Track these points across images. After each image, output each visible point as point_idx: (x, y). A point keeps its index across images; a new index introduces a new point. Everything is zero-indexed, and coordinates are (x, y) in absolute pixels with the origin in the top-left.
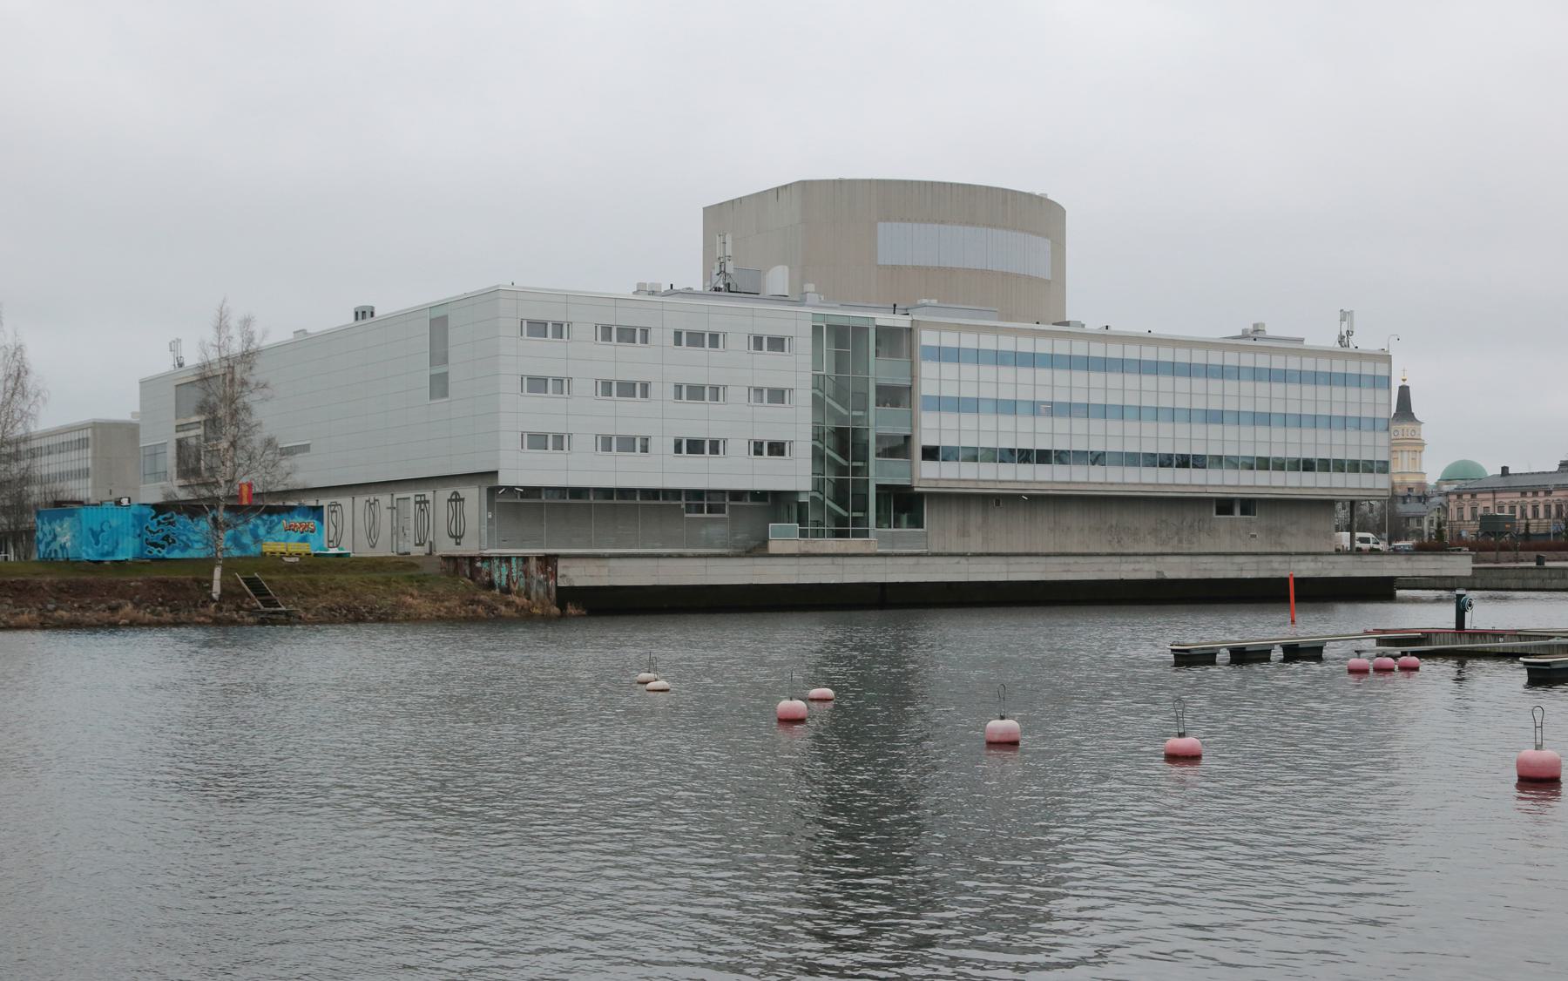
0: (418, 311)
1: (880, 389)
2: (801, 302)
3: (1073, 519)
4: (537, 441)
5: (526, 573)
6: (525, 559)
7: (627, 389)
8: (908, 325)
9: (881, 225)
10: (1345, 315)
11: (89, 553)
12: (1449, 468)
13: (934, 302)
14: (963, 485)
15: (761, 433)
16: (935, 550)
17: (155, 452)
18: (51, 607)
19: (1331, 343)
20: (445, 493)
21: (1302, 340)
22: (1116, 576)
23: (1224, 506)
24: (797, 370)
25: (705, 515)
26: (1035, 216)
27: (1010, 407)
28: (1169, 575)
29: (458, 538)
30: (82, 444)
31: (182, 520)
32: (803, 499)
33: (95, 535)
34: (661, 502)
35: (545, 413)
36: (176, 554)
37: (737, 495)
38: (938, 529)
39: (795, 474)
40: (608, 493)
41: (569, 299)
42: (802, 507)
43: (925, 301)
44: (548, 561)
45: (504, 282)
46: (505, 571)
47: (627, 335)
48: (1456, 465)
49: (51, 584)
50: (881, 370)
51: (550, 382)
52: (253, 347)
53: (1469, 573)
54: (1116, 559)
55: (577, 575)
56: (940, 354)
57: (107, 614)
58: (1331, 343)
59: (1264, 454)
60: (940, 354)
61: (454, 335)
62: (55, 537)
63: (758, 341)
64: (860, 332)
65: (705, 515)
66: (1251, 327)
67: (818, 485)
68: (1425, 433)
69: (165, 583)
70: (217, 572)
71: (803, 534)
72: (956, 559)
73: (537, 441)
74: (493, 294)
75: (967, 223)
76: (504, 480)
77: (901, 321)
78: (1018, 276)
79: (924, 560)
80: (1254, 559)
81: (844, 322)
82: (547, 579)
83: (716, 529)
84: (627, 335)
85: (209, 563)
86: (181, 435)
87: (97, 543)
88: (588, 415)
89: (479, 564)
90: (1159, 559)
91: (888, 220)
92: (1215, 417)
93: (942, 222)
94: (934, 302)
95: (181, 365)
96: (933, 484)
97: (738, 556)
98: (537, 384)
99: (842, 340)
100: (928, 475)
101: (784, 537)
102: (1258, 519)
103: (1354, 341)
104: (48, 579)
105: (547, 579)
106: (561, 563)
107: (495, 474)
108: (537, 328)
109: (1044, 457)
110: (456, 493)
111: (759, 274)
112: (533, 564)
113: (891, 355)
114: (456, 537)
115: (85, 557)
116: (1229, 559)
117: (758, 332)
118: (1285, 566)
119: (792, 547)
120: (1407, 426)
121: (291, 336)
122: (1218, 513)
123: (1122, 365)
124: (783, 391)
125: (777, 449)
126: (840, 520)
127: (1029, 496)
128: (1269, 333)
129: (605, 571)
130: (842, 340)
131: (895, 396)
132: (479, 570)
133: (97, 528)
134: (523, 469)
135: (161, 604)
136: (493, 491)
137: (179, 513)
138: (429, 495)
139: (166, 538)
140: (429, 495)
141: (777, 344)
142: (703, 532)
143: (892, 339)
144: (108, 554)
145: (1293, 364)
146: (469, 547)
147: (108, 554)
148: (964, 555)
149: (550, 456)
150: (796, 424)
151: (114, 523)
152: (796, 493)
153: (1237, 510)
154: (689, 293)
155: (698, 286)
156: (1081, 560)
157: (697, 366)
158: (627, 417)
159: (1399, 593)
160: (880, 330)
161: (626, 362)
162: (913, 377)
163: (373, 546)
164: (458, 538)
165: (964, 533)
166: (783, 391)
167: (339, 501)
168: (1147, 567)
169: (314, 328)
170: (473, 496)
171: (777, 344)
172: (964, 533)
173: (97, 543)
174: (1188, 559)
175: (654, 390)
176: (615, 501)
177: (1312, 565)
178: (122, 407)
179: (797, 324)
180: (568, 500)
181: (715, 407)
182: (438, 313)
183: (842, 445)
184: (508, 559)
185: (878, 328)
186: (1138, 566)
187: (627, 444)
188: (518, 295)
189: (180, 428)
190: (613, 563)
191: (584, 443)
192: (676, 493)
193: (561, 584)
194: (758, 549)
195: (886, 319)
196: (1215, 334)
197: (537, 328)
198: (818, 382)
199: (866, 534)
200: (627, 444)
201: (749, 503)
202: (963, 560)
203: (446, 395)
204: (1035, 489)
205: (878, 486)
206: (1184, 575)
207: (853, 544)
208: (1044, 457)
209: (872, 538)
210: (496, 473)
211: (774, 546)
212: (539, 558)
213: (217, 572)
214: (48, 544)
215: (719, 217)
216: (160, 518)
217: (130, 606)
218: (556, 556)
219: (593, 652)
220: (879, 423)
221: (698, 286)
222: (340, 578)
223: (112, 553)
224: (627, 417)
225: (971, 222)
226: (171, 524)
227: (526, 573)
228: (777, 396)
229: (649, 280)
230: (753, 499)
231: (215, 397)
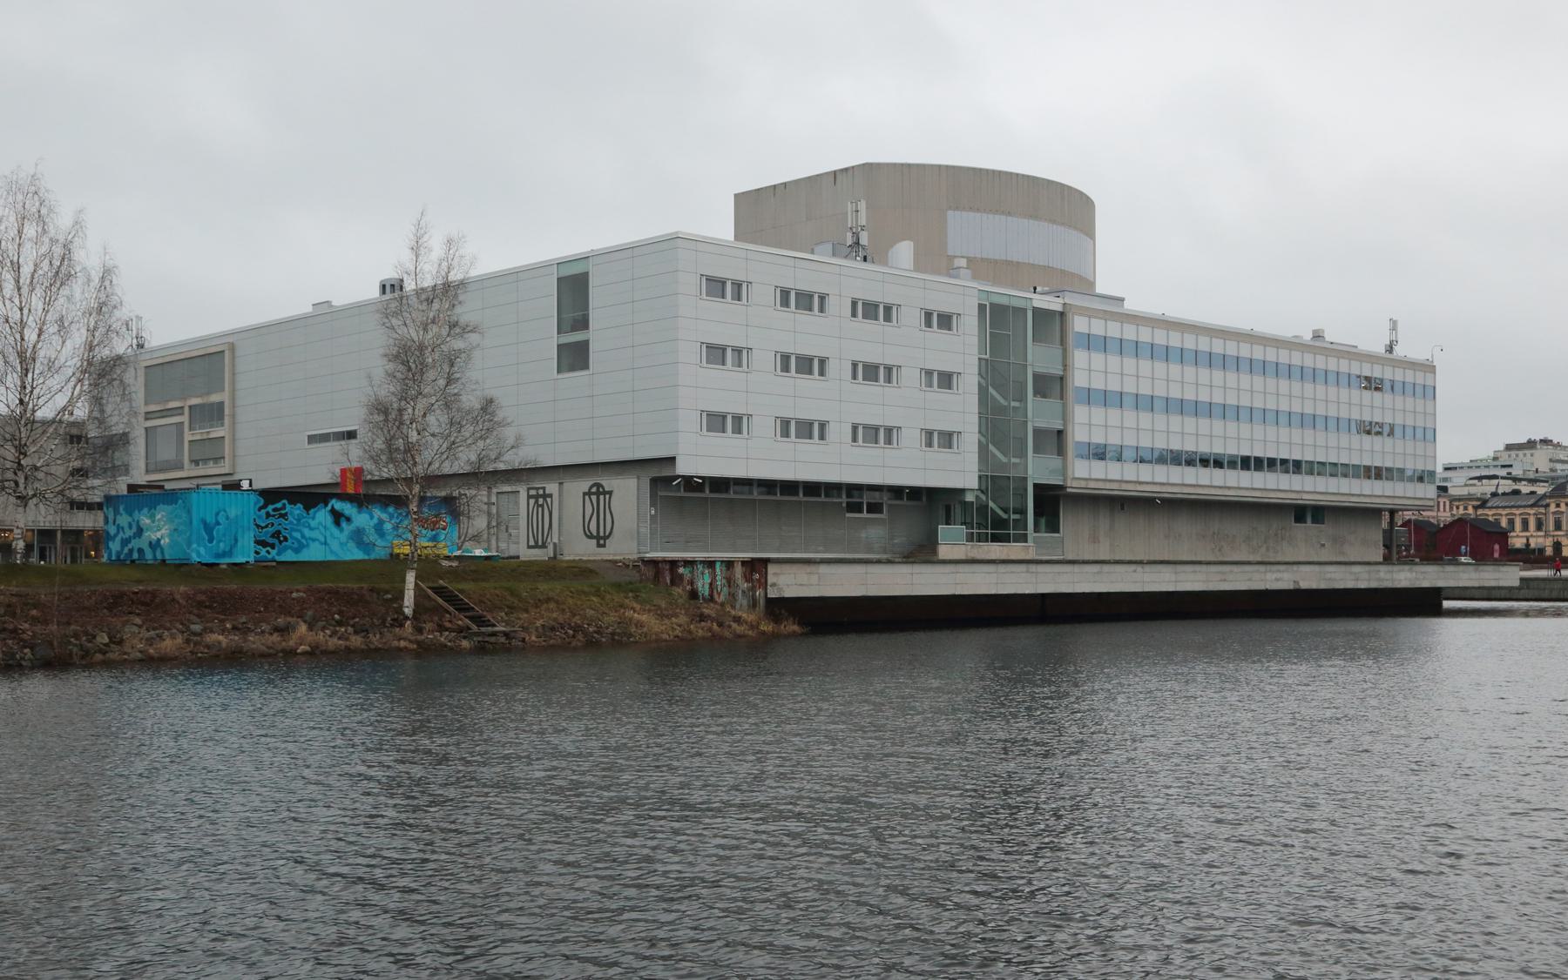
0: (546, 266)
1: (1038, 378)
3: (1185, 526)
6: (729, 564)
8: (1059, 308)
9: (950, 213)
10: (1394, 325)
11: (200, 553)
14: (1108, 486)
16: (1070, 557)
18: (197, 628)
19: (1380, 349)
20: (577, 487)
23: (1302, 513)
24: (962, 351)
28: (1304, 585)
29: (601, 540)
31: (296, 510)
32: (970, 498)
33: (209, 529)
34: (823, 499)
35: (721, 389)
36: (289, 556)
37: (897, 491)
38: (1075, 533)
39: (959, 471)
40: (768, 485)
42: (966, 506)
44: (756, 567)
46: (707, 580)
49: (187, 597)
50: (1040, 358)
51: (729, 351)
52: (455, 276)
53: (1517, 583)
54: (1262, 568)
55: (789, 583)
56: (1089, 342)
57: (276, 637)
58: (1380, 349)
59: (1367, 462)
60: (1089, 342)
62: (140, 532)
65: (865, 515)
69: (335, 593)
70: (411, 577)
71: (970, 538)
72: (1133, 567)
74: (673, 240)
75: (1031, 217)
76: (683, 468)
77: (1054, 304)
78: (1073, 275)
79: (1106, 568)
80: (1367, 568)
82: (753, 589)
83: (875, 532)
85: (396, 564)
87: (211, 541)
88: (765, 394)
89: (681, 570)
90: (1295, 568)
91: (957, 208)
92: (1308, 421)
93: (1009, 214)
95: (141, 346)
96: (1083, 484)
97: (889, 562)
98: (716, 353)
100: (1083, 473)
101: (952, 541)
102: (1327, 529)
103: (1399, 351)
104: (182, 588)
105: (753, 589)
107: (671, 460)
108: (716, 286)
110: (598, 485)
113: (1429, 393)
114: (598, 538)
115: (195, 558)
116: (1348, 568)
117: (930, 307)
118: (1388, 576)
119: (959, 552)
121: (309, 309)
127: (1164, 500)
133: (210, 519)
134: (703, 457)
135: (340, 623)
136: (656, 482)
137: (292, 502)
138: (552, 488)
139: (277, 534)
140: (552, 488)
142: (863, 535)
144: (224, 555)
147: (224, 555)
148: (1140, 562)
150: (961, 411)
151: (233, 513)
152: (962, 491)
156: (1235, 568)
159: (1447, 604)
162: (1065, 366)
164: (601, 540)
165: (1095, 540)
168: (1286, 576)
169: (338, 301)
170: (627, 493)
171: (946, 321)
172: (1095, 540)
173: (211, 541)
174: (1317, 568)
176: (732, 495)
177: (1409, 575)
179: (963, 296)
180: (779, 497)
181: (889, 391)
184: (711, 564)
185: (1035, 309)
186: (1279, 575)
187: (806, 429)
190: (823, 569)
191: (763, 426)
194: (923, 552)
200: (806, 429)
202: (1139, 568)
203: (585, 366)
205: (1036, 486)
209: (1030, 543)
210: (672, 460)
211: (944, 551)
212: (744, 563)
213: (411, 577)
214: (125, 542)
216: (270, 508)
217: (303, 628)
218: (766, 561)
222: (543, 586)
223: (230, 553)
225: (1034, 216)
226: (284, 516)
227: (730, 581)
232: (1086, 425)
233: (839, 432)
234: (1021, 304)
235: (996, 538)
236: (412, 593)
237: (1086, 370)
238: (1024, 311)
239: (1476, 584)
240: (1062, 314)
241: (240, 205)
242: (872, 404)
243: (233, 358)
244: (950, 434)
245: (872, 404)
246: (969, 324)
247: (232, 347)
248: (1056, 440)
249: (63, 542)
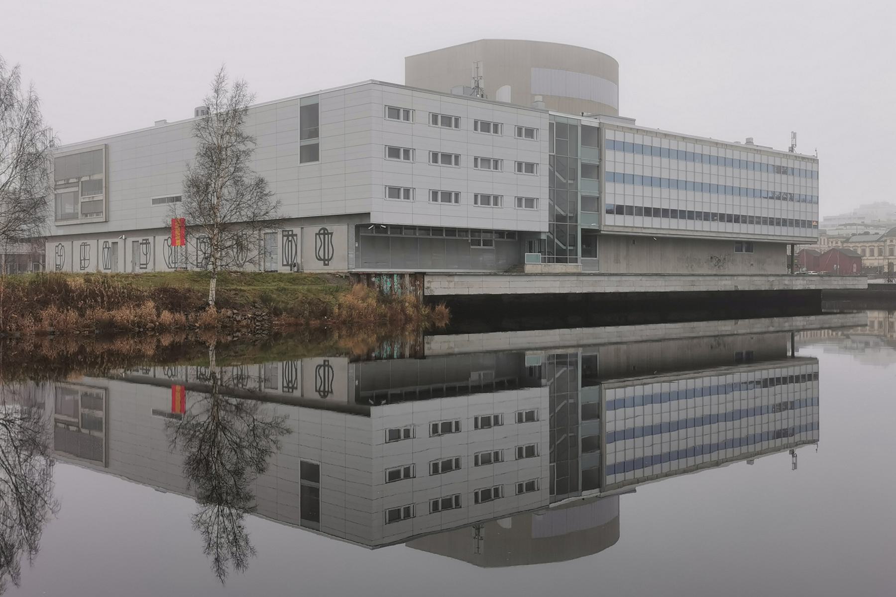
4: (394, 192)
5: (402, 286)
6: (402, 276)
14: (735, 236)
25: (482, 247)
27: (652, 182)
32: (543, 237)
35: (398, 173)
37: (501, 233)
39: (537, 221)
44: (417, 277)
54: (716, 278)
56: (614, 145)
58: (785, 149)
60: (614, 145)
63: (435, 118)
65: (482, 247)
73: (394, 192)
76: (374, 220)
77: (594, 123)
81: (564, 121)
88: (422, 176)
89: (373, 279)
94: (855, 266)
97: (495, 275)
100: (612, 223)
101: (533, 262)
106: (427, 279)
109: (737, 219)
110: (325, 229)
112: (407, 279)
113: (814, 175)
114: (324, 260)
123: (669, 153)
126: (561, 252)
129: (452, 285)
131: (593, 171)
132: (373, 283)
134: (388, 213)
140: (297, 230)
141: (530, 133)
145: (629, 138)
149: (400, 204)
150: (538, 186)
152: (540, 233)
164: (326, 261)
171: (530, 133)
172: (617, 261)
184: (391, 276)
187: (447, 197)
193: (427, 293)
194: (516, 268)
195: (586, 121)
196: (730, 139)
199: (576, 261)
200: (447, 197)
206: (557, 291)
207: (570, 267)
208: (737, 219)
211: (528, 268)
212: (411, 275)
218: (424, 274)
227: (402, 286)
235: (559, 261)
240: (598, 129)
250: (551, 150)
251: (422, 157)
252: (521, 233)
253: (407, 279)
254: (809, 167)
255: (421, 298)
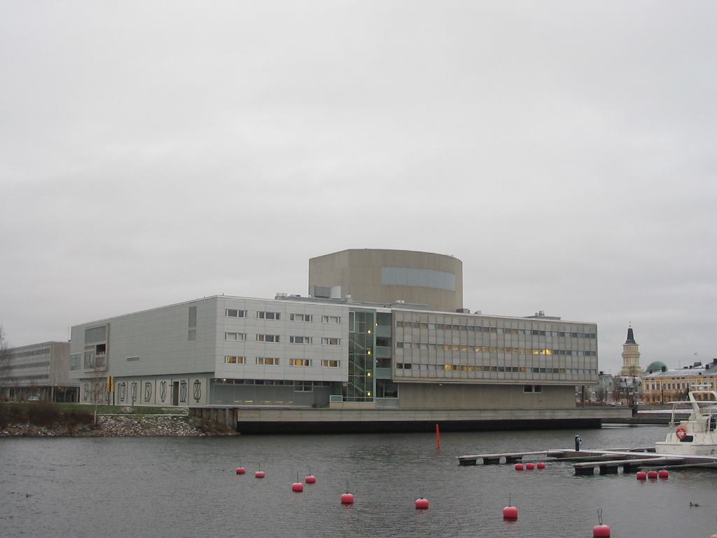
2: (344, 302)
7: (270, 338)
12: (658, 362)
13: (403, 302)
15: (327, 359)
17: (77, 357)
20: (193, 381)
21: (559, 318)
22: (479, 419)
23: (528, 388)
24: (342, 331)
26: (447, 266)
29: (198, 399)
30: (47, 351)
32: (345, 385)
37: (316, 383)
41: (245, 301)
43: (399, 301)
44: (234, 411)
45: (218, 293)
47: (270, 316)
48: (652, 365)
55: (243, 417)
60: (401, 324)
61: (199, 315)
64: (370, 315)
66: (538, 312)
67: (351, 379)
68: (640, 349)
74: (213, 300)
76: (217, 376)
77: (388, 310)
81: (363, 311)
84: (270, 316)
86: (86, 351)
94: (403, 302)
99: (362, 318)
100: (399, 375)
101: (336, 402)
106: (239, 412)
108: (232, 313)
110: (197, 381)
111: (329, 290)
112: (227, 412)
113: (594, 336)
120: (633, 347)
122: (525, 391)
124: (336, 340)
125: (334, 364)
128: (546, 315)
130: (362, 318)
134: (226, 372)
136: (212, 381)
138: (187, 381)
143: (385, 319)
146: (203, 404)
150: (342, 353)
152: (341, 383)
153: (534, 390)
154: (298, 298)
155: (305, 294)
157: (300, 329)
158: (270, 350)
160: (379, 314)
161: (271, 327)
163: (163, 401)
166: (336, 340)
167: (150, 381)
170: (204, 382)
175: (281, 339)
178: (64, 336)
179: (343, 311)
182: (192, 305)
183: (358, 361)
185: (378, 313)
187: (270, 361)
188: (224, 299)
189: (86, 348)
192: (291, 382)
195: (380, 310)
197: (232, 313)
198: (351, 336)
200: (270, 361)
201: (322, 386)
204: (512, 382)
205: (377, 380)
210: (213, 373)
211: (332, 405)
212: (230, 409)
215: (317, 264)
218: (237, 408)
219: (253, 454)
220: (375, 353)
221: (305, 294)
224: (270, 350)
228: (334, 341)
229: (281, 292)
230: (324, 385)
231: (98, 339)
232: (399, 355)
233: (284, 362)
234: (371, 312)
235: (359, 400)
236: (685, 410)
237: (399, 335)
238: (372, 314)
239: (606, 417)
240: (391, 314)
241: (32, 305)
242: (299, 351)
243: (109, 328)
244: (336, 362)
245: (299, 351)
246: (346, 320)
247: (109, 325)
248: (385, 363)
249: (376, 372)
250: (351, 328)
251: (285, 340)
252: (333, 383)
253: (227, 412)
254: (582, 344)
255: (236, 423)
